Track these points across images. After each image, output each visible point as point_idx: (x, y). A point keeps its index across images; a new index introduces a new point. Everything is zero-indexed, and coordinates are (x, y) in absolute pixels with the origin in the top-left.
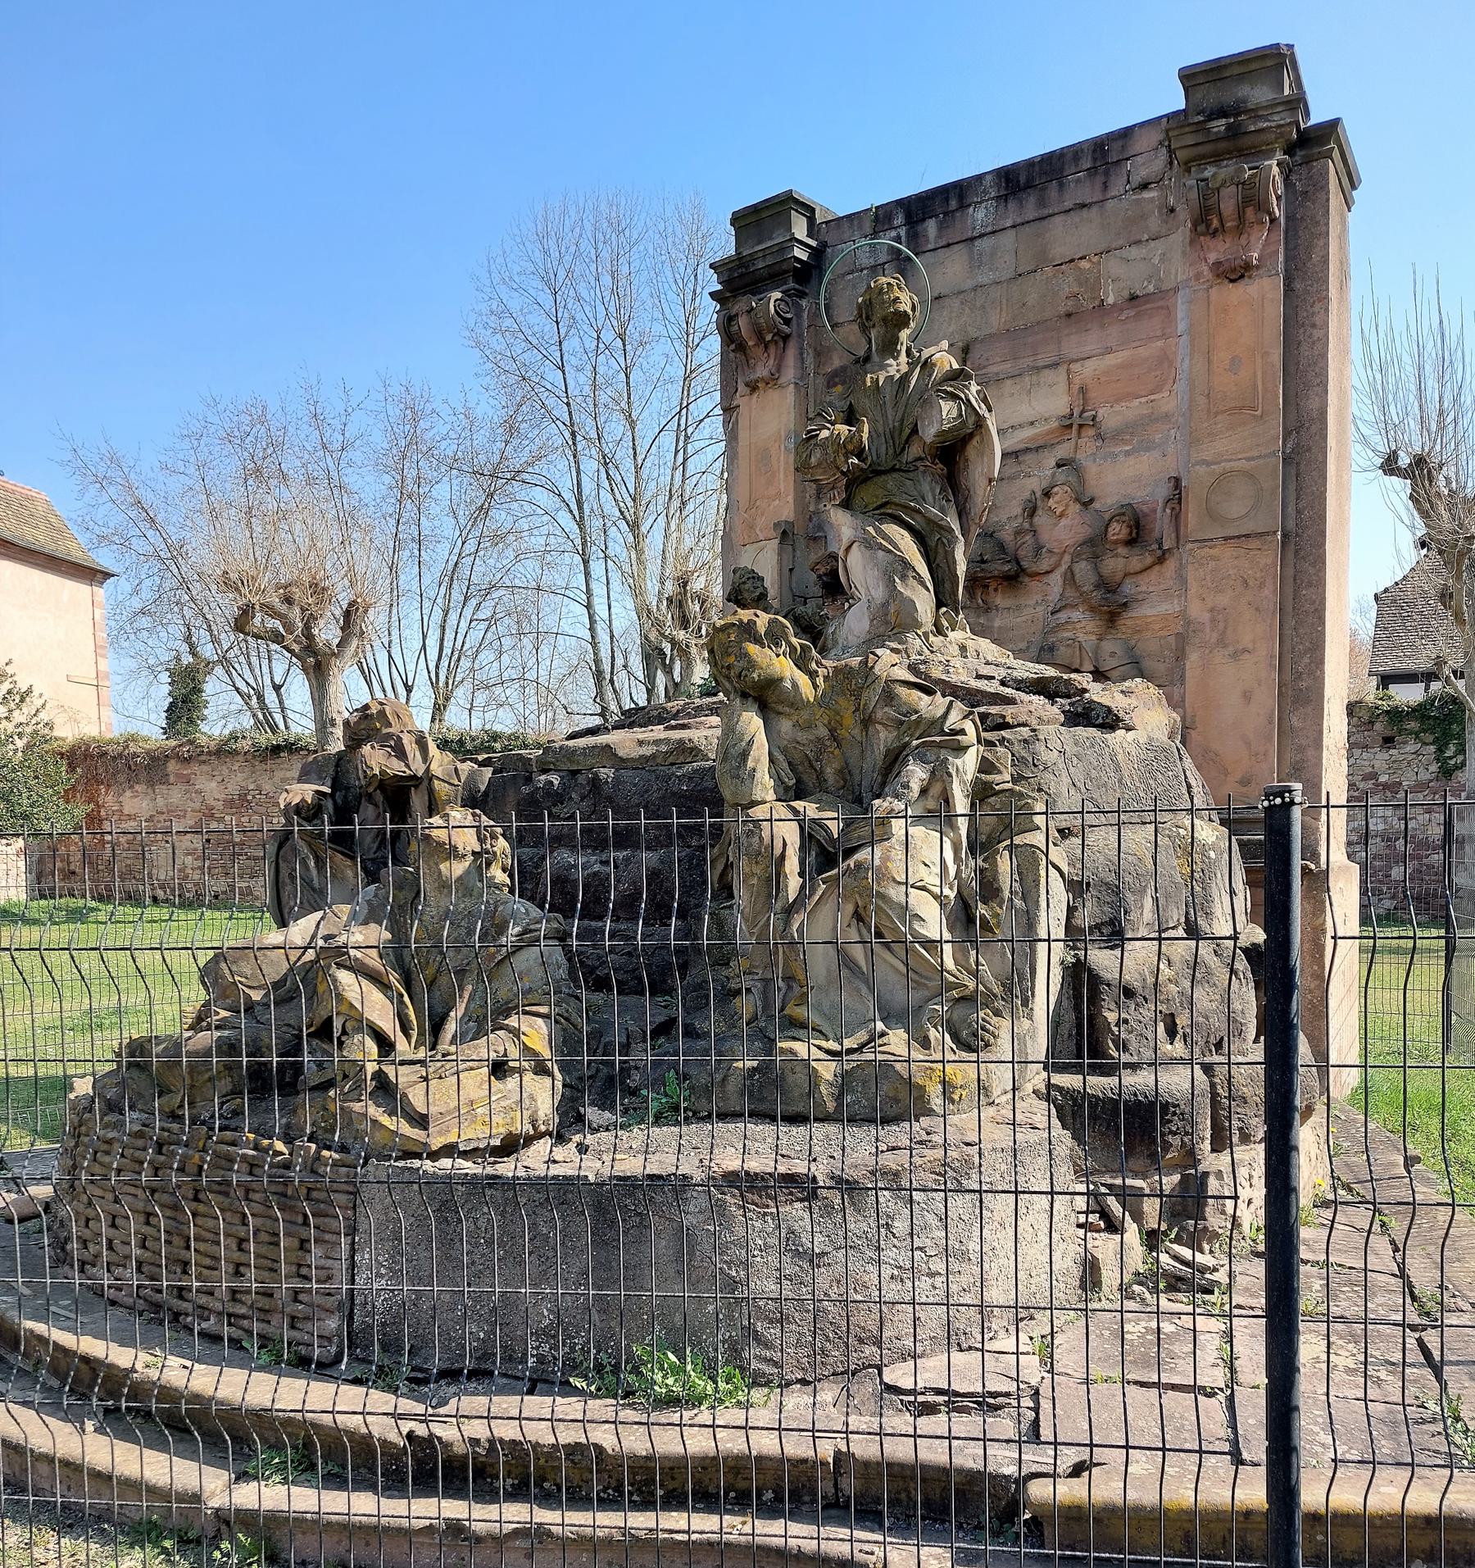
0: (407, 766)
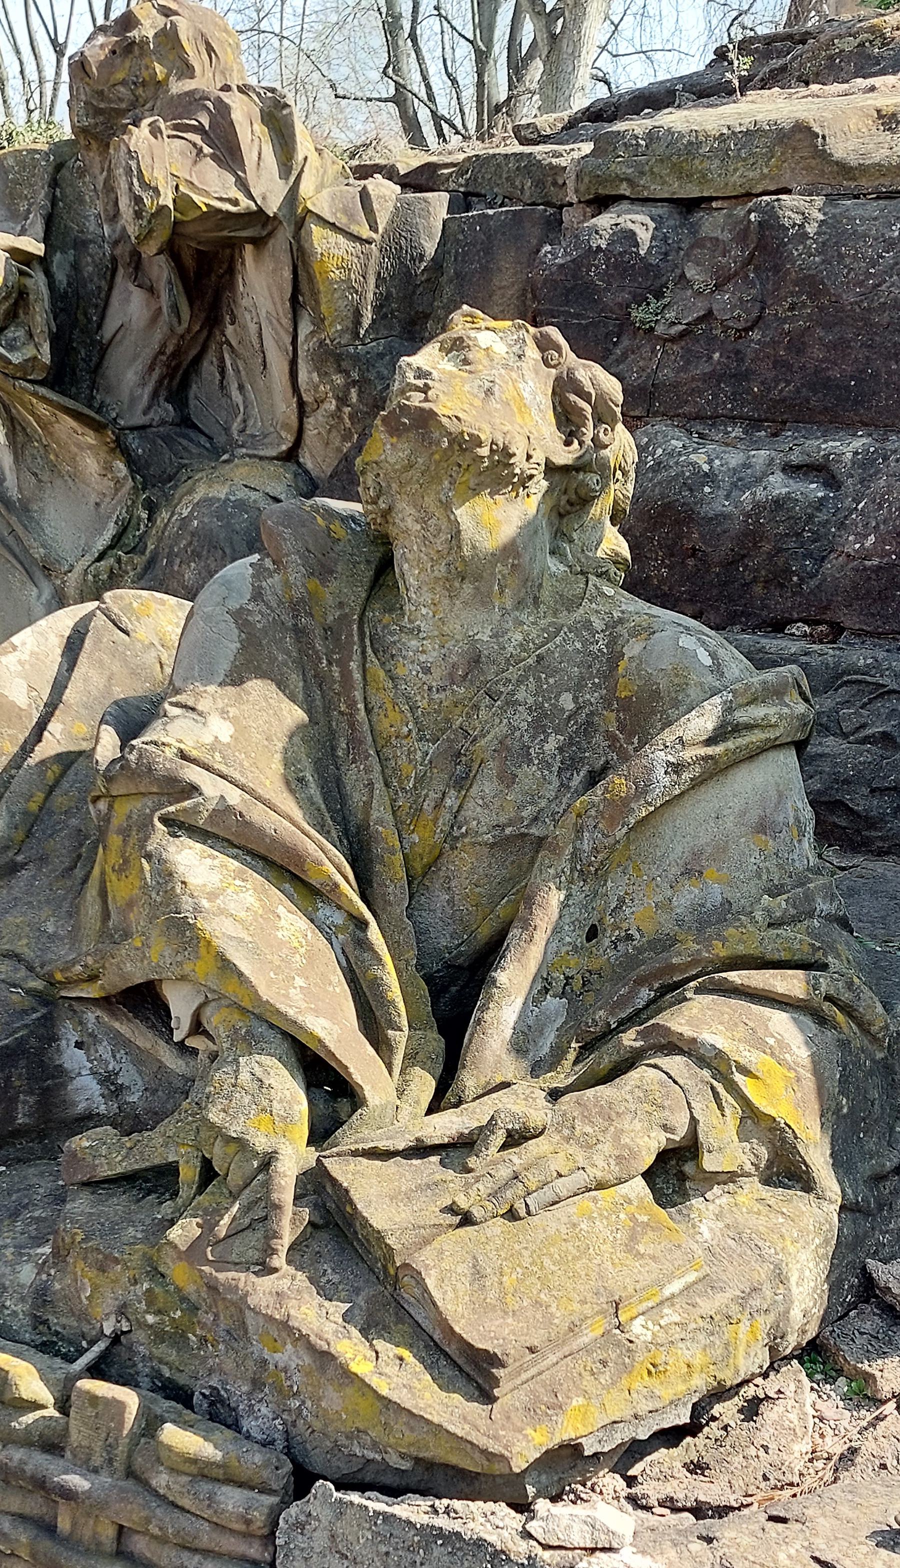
0: (243, 185)
